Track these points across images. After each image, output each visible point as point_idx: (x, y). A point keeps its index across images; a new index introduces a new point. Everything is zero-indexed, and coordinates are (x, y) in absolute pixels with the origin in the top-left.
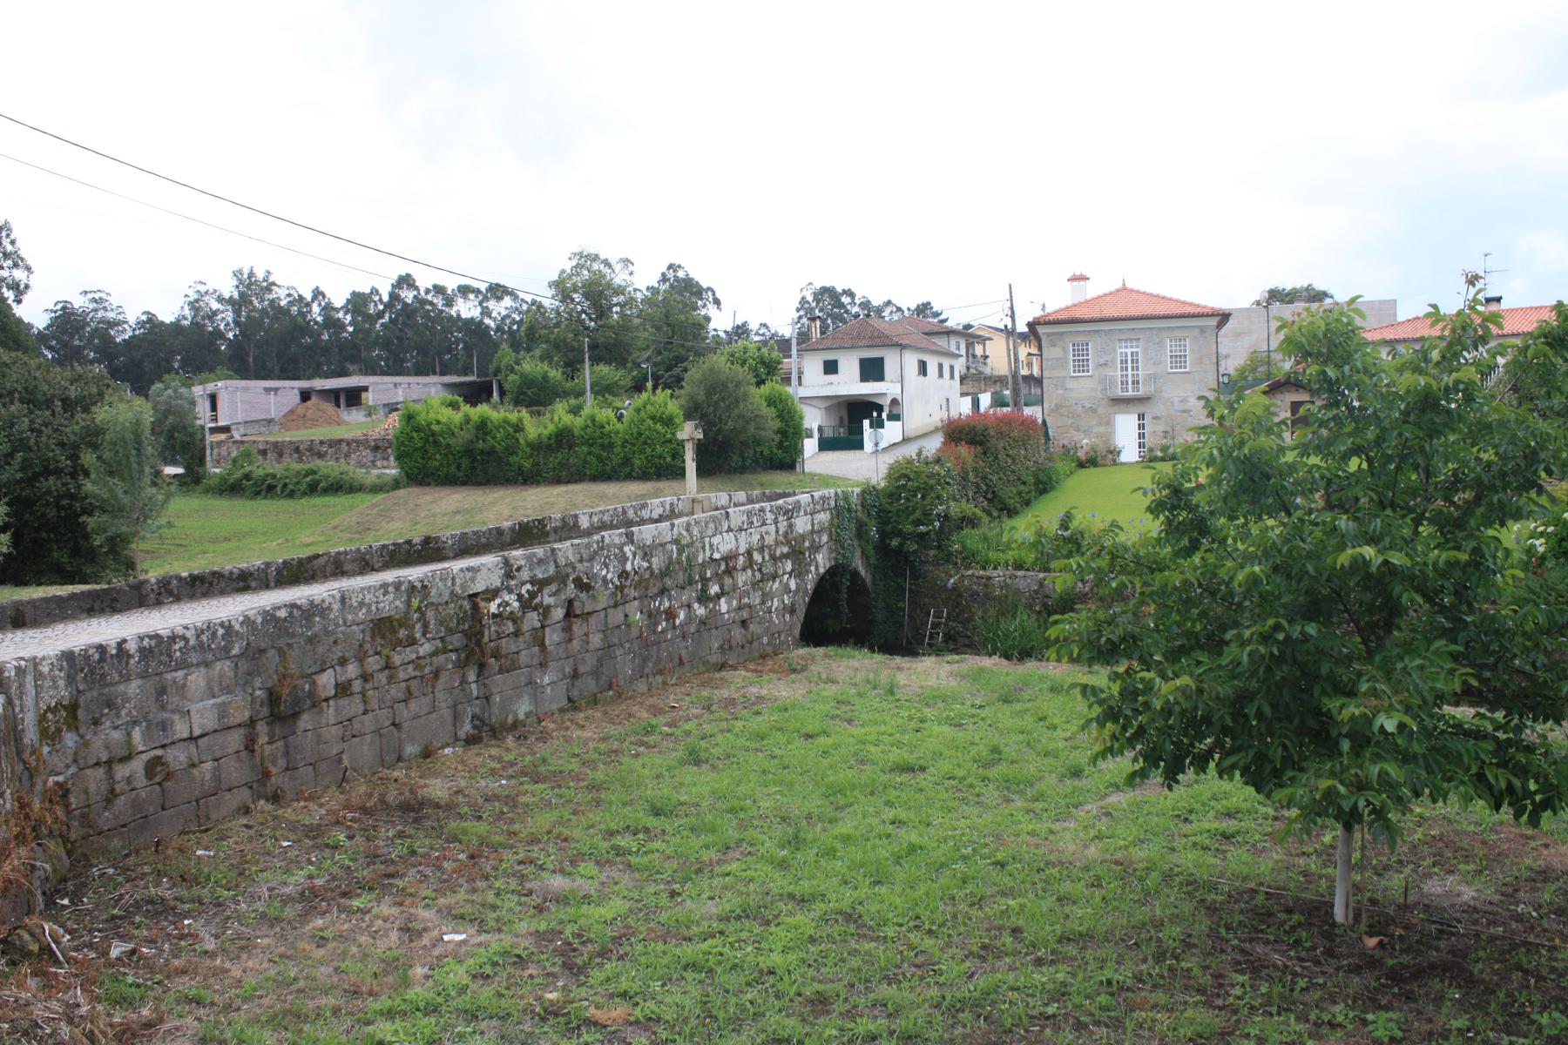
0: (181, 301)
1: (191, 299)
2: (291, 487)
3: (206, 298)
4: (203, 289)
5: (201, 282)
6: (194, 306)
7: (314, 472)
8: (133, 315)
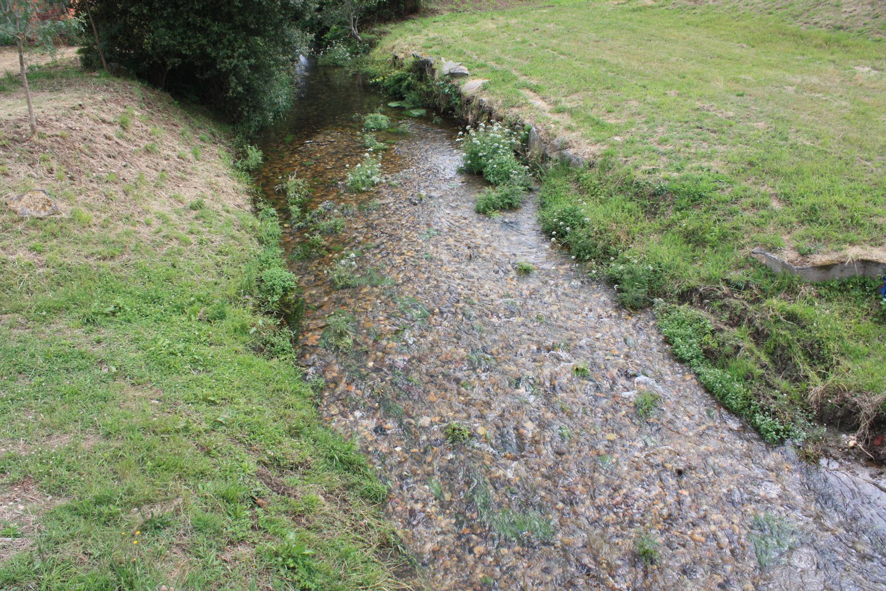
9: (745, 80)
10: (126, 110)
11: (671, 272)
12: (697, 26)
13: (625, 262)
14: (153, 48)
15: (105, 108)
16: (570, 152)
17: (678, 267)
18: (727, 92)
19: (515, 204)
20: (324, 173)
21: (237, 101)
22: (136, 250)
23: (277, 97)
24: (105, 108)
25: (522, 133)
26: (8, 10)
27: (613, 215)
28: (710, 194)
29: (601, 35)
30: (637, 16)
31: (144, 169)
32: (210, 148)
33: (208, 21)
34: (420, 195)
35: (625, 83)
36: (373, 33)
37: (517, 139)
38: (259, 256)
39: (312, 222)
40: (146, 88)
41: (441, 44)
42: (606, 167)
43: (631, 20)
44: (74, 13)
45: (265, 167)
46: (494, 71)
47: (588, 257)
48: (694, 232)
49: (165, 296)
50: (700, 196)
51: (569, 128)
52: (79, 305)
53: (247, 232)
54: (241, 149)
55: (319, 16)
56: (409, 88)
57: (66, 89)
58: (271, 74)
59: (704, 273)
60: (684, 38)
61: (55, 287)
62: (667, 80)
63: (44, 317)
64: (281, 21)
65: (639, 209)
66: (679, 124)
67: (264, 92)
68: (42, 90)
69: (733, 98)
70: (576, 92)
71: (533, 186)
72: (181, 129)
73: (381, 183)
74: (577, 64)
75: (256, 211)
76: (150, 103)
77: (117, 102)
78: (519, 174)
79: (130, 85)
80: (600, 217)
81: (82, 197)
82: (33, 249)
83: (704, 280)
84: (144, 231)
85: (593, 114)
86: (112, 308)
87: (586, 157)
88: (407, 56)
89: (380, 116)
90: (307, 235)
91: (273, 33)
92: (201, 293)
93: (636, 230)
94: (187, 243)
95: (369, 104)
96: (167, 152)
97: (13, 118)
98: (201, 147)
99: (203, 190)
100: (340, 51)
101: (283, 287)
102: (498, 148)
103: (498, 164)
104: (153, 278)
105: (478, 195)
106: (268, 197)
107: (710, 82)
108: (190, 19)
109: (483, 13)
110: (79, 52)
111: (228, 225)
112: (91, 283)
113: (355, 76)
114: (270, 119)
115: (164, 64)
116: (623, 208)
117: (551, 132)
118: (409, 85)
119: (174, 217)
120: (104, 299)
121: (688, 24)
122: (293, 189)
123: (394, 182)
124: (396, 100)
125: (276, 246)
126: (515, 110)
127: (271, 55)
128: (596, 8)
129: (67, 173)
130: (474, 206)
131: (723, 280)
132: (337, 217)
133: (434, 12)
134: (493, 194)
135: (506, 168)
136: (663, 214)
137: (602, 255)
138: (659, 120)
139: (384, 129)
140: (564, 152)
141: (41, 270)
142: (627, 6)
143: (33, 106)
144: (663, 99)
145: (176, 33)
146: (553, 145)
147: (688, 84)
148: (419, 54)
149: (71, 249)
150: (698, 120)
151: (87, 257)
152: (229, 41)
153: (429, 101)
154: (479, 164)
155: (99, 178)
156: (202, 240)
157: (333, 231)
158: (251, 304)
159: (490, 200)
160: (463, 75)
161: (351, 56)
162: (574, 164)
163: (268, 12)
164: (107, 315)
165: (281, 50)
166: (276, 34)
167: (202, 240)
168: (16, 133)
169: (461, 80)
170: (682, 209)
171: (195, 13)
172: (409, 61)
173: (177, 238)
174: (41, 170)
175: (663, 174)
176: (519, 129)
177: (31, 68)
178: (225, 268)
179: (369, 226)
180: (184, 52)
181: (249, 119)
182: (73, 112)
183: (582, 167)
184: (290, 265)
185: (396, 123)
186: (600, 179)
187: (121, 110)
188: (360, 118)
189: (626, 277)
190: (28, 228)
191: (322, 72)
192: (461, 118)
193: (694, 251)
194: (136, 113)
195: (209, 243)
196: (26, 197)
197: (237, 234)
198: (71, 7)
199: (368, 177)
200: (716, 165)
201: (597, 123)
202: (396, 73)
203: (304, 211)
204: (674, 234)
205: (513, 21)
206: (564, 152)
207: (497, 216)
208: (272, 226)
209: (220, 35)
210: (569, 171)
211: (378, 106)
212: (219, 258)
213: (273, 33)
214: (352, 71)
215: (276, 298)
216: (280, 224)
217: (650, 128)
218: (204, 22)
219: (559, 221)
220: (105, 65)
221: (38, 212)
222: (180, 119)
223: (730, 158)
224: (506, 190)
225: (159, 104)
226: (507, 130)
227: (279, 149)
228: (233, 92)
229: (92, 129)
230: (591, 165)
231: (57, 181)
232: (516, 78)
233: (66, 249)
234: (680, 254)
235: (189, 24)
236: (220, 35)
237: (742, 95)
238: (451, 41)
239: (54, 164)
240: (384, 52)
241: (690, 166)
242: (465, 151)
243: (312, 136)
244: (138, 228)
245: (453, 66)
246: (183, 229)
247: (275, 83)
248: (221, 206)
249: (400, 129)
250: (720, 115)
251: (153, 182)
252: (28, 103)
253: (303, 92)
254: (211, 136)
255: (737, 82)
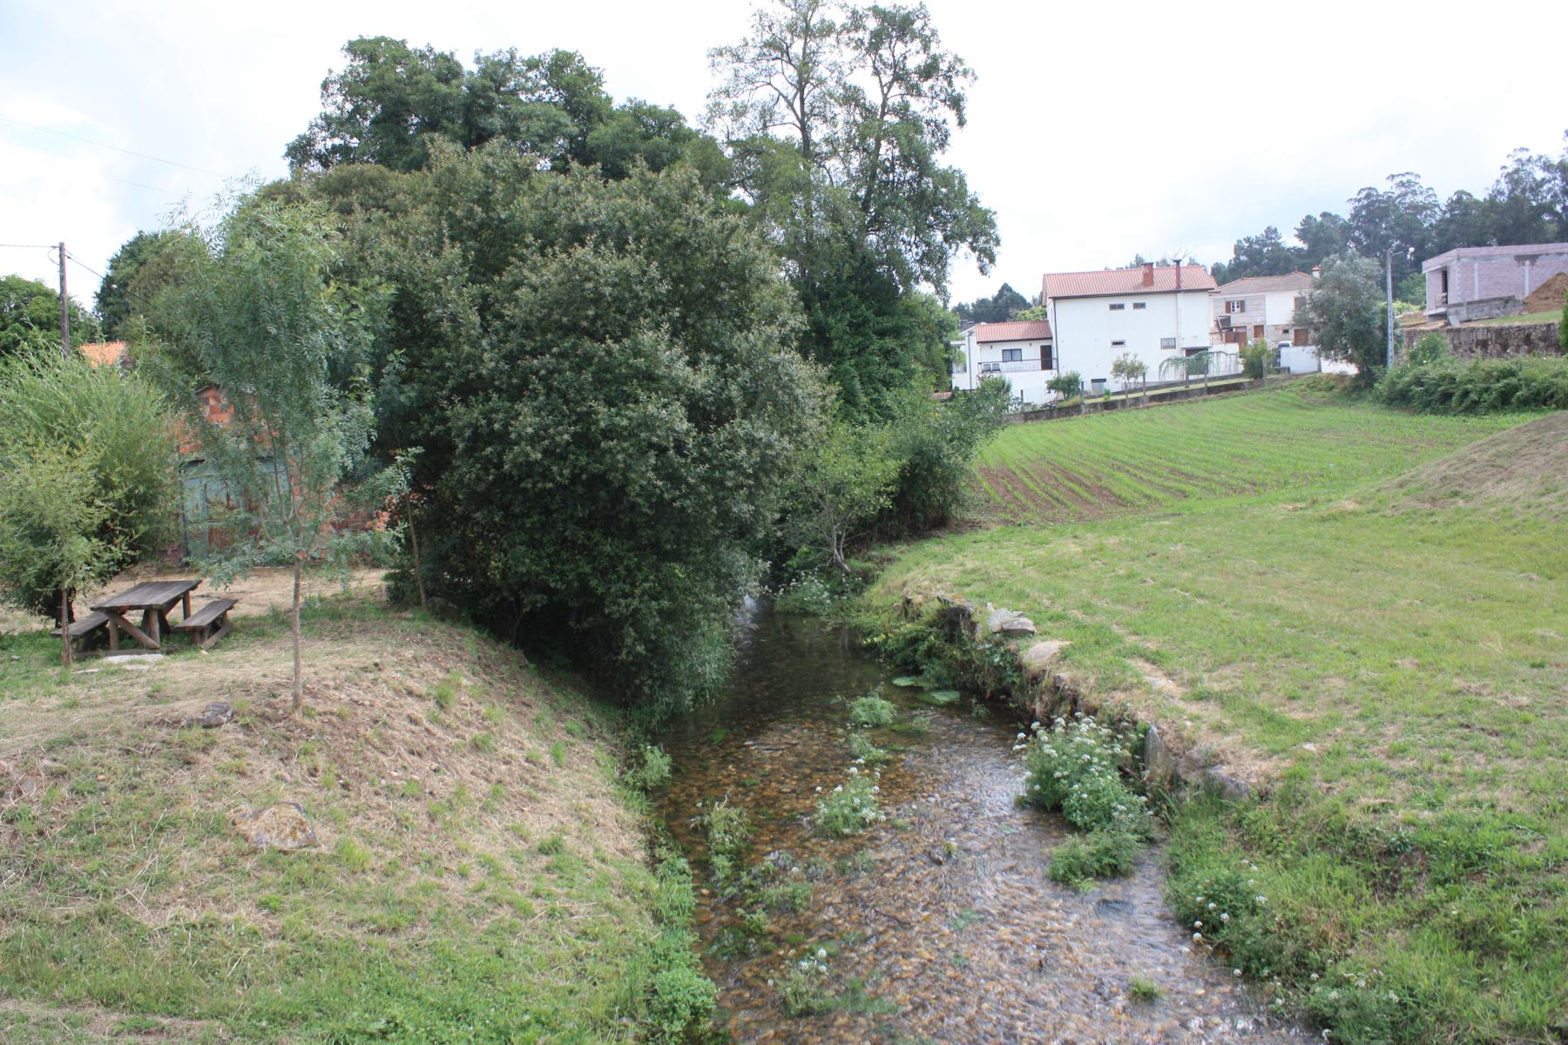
0: (1498, 174)
1: (1510, 170)
2: (1473, 396)
3: (1528, 168)
4: (1524, 156)
5: (1523, 149)
6: (1514, 178)
7: (1512, 374)
8: (1444, 196)
9: (1543, 638)
10: (448, 676)
11: (1438, 1007)
12: (1440, 544)
13: (1340, 983)
14: (504, 576)
15: (415, 670)
16: (1223, 771)
17: (1450, 997)
18: (1511, 660)
19: (1124, 866)
20: (776, 799)
21: (634, 669)
22: (439, 920)
23: (703, 664)
24: (415, 670)
25: (1132, 735)
26: (291, 515)
27: (1311, 891)
28: (1500, 853)
29: (1268, 562)
30: (1330, 529)
31: (467, 776)
32: (582, 746)
33: (596, 536)
34: (948, 846)
35: (1318, 646)
36: (870, 559)
37: (1124, 747)
38: (652, 946)
39: (751, 887)
40: (485, 640)
41: (986, 580)
42: (1291, 800)
43: (1319, 536)
44: (387, 519)
45: (675, 786)
46: (1080, 627)
47: (1266, 972)
48: (1475, 928)
49: (479, 1009)
50: (1481, 857)
51: (1218, 728)
52: (326, 1012)
53: (634, 900)
54: (634, 751)
55: (779, 534)
56: (931, 653)
57: (357, 638)
58: (694, 626)
59: (1508, 1013)
60: (1420, 566)
61: (291, 976)
62: (1394, 639)
63: (263, 1030)
64: (716, 538)
65: (1361, 880)
66: (1425, 720)
67: (680, 654)
68: (321, 638)
69: (1525, 670)
70: (1229, 662)
71: (1156, 833)
72: (536, 711)
73: (876, 820)
74: (1226, 614)
75: (653, 863)
76: (488, 666)
77: (436, 662)
78: (1129, 811)
79: (460, 635)
80: (1286, 894)
81: (359, 819)
82: (263, 905)
83: (1508, 1026)
84: (453, 884)
85: (1261, 702)
86: (381, 1025)
87: (1254, 780)
88: (927, 599)
89: (879, 702)
90: (740, 911)
91: (701, 558)
92: (544, 1007)
93: (1358, 921)
94: (527, 914)
95: (860, 681)
96: (508, 750)
97: (268, 681)
98: (567, 744)
99: (564, 820)
100: (813, 589)
101: (693, 1007)
102: (1090, 763)
103: (1090, 793)
104: (461, 974)
105: (1054, 850)
106: (675, 837)
107: (1475, 642)
108: (567, 534)
109: (1059, 527)
110: (387, 578)
111: (601, 885)
112: (352, 974)
113: (837, 631)
114: (688, 701)
115: (519, 602)
116: (1329, 877)
117: (1185, 734)
118: (930, 649)
119: (509, 864)
120: (372, 1005)
121: (1423, 541)
122: (721, 826)
123: (900, 822)
124: (907, 673)
125: (685, 928)
126: (1119, 695)
127: (697, 595)
128: (1255, 517)
129: (339, 778)
130: (1048, 870)
131: (1552, 1029)
132: (796, 880)
133: (974, 525)
134: (1083, 847)
135: (1105, 800)
136: (1409, 889)
137: (1294, 969)
138: (1386, 712)
139: (886, 724)
140: (1212, 772)
141: (271, 944)
142: (1310, 512)
143: (302, 662)
144: (1391, 675)
145: (543, 554)
146: (1190, 759)
147: (1435, 647)
148: (948, 597)
149: (327, 910)
150: (1461, 712)
151: (351, 926)
152: (628, 569)
153: (965, 678)
154: (1055, 793)
155: (391, 789)
156: (553, 910)
157: (787, 907)
158: (631, 1035)
159: (1077, 858)
160: (1024, 633)
161: (831, 598)
162: (1232, 795)
163: (695, 524)
164: (372, 1036)
165: (712, 586)
166: (708, 561)
167: (553, 910)
168: (269, 705)
169: (1022, 642)
170: (1447, 880)
171: (576, 524)
172: (930, 609)
173: (510, 904)
174: (298, 769)
175: (1402, 814)
176: (1126, 728)
177: (309, 603)
178: (590, 964)
179: (853, 899)
180: (552, 585)
181: (651, 700)
182: (364, 675)
183: (1246, 799)
184: (709, 966)
185: (905, 716)
186: (1281, 823)
187: (441, 675)
188: (843, 704)
189: (1345, 1014)
190: (261, 867)
191: (780, 625)
192: (1023, 708)
193: (1480, 965)
194: (465, 682)
195: (566, 916)
196: (266, 813)
197: (617, 903)
198: (384, 509)
199: (855, 810)
200: (1505, 796)
201: (1271, 719)
202: (908, 627)
203: (737, 868)
204: (1434, 931)
205: (1112, 540)
206: (1212, 772)
207: (1090, 887)
208: (679, 891)
209: (615, 560)
210: (1223, 808)
211: (876, 683)
212: (580, 945)
213: (701, 558)
214: (832, 622)
215: (678, 1026)
216: (694, 889)
217: (1370, 727)
218: (589, 538)
219: (1207, 901)
220: (423, 601)
221: (283, 840)
222: (536, 694)
223: (1532, 784)
224: (1106, 841)
225: (504, 668)
226: (1105, 731)
227: (700, 755)
228: (629, 653)
229: (390, 705)
230: (1264, 797)
231: (321, 789)
232: (1119, 639)
233: (318, 909)
234: (1452, 973)
235: (565, 540)
236: (615, 560)
237: (1541, 666)
238: (1004, 574)
239: (321, 761)
240: (889, 592)
241: (1454, 798)
242: (1030, 767)
243: (759, 733)
244: (446, 880)
245: (1007, 618)
246: (523, 888)
247: (701, 640)
248: (591, 850)
249: (915, 724)
250: (1503, 703)
251: (479, 800)
252: (296, 658)
253: (747, 656)
254: (585, 726)
255: (1529, 642)
